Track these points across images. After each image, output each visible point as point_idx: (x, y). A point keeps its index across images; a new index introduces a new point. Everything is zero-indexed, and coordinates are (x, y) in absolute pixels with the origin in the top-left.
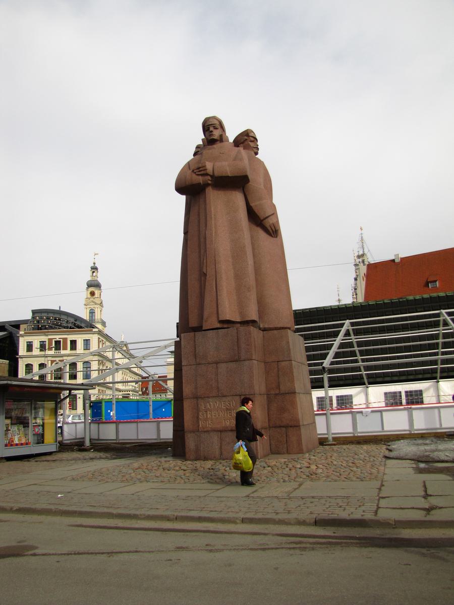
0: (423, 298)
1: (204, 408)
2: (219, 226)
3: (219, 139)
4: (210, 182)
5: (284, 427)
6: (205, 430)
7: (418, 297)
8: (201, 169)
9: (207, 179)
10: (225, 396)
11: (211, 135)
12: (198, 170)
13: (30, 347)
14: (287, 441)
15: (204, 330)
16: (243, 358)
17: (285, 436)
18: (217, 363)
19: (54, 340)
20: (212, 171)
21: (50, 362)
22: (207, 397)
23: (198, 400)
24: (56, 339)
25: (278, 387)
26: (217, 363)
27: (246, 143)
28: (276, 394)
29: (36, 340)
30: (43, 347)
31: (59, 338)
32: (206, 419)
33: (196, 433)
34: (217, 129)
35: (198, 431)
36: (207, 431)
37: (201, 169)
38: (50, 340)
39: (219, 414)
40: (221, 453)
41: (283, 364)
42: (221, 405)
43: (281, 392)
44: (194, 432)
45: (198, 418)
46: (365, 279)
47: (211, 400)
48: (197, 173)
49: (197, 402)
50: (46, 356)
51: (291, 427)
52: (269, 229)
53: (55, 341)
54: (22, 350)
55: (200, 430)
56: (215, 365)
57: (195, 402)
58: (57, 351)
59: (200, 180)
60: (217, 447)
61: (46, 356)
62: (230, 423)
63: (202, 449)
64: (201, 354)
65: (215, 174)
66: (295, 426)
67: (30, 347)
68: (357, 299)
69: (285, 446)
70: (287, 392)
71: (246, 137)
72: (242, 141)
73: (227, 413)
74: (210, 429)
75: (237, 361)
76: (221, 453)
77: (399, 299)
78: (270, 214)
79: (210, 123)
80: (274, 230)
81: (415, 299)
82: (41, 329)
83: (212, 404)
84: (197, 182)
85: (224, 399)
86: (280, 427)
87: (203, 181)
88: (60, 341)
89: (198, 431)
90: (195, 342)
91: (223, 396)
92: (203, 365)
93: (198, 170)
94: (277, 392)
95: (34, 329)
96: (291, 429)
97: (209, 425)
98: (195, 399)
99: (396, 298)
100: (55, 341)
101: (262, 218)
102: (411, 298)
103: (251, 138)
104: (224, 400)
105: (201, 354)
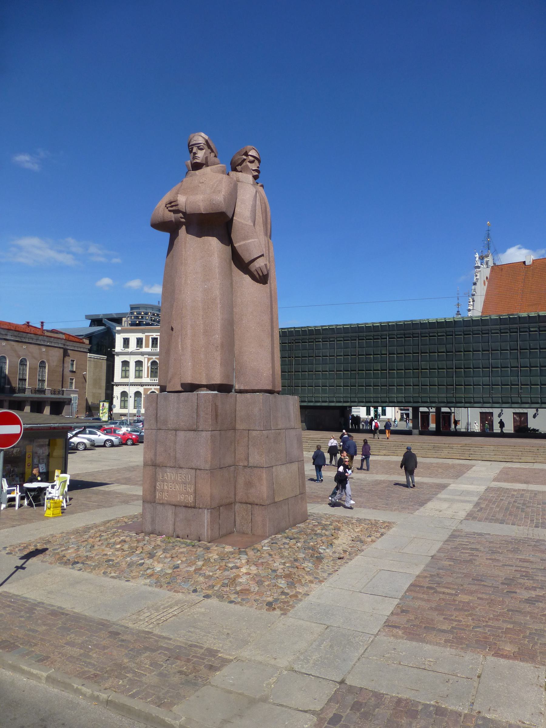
0: (539, 316)
1: (161, 478)
2: (190, 273)
3: (204, 162)
4: (183, 220)
5: (250, 504)
6: (161, 502)
7: (533, 314)
8: (173, 204)
9: (179, 216)
10: (181, 468)
11: (194, 158)
12: (170, 205)
13: (126, 342)
14: (252, 520)
15: (168, 392)
16: (200, 428)
17: (250, 514)
18: (176, 430)
19: (150, 337)
20: (184, 207)
21: (146, 359)
22: (165, 467)
23: (156, 469)
24: (153, 335)
25: (247, 459)
26: (176, 430)
27: (244, 164)
28: (245, 466)
29: (133, 338)
30: (139, 342)
31: (156, 335)
32: (162, 491)
33: (153, 504)
34: (202, 149)
35: (154, 502)
36: (162, 504)
37: (173, 204)
38: (147, 337)
39: (175, 486)
40: (174, 529)
41: (254, 433)
42: (178, 477)
43: (250, 465)
44: (151, 503)
45: (155, 487)
46: (487, 283)
47: (168, 470)
48: (170, 209)
49: (155, 472)
50: (142, 354)
51: (257, 505)
52: (255, 273)
53: (152, 338)
54: (119, 346)
55: (156, 502)
56: (174, 432)
57: (154, 470)
58: (154, 349)
59: (171, 217)
60: (171, 522)
61: (142, 354)
62: (185, 499)
63: (157, 522)
64: (162, 419)
65: (187, 211)
66: (261, 505)
67: (126, 342)
68: (473, 306)
69: (250, 524)
70: (255, 465)
71: (244, 157)
72: (240, 161)
73: (182, 487)
74: (165, 502)
75: (196, 431)
76: (174, 529)
77: (509, 315)
78: (255, 256)
79: (194, 142)
80: (261, 274)
81: (529, 316)
82: (139, 324)
83: (170, 474)
84: (169, 220)
85: (180, 471)
86: (246, 503)
87: (175, 219)
88: (157, 338)
89: (154, 502)
90: (157, 404)
91: (180, 468)
92: (163, 431)
93: (170, 205)
94: (246, 464)
95: (132, 325)
96: (257, 507)
97: (165, 497)
98: (154, 467)
99: (506, 314)
100: (152, 338)
101: (246, 262)
102: (524, 315)
103: (250, 157)
104: (180, 472)
105: (162, 419)
